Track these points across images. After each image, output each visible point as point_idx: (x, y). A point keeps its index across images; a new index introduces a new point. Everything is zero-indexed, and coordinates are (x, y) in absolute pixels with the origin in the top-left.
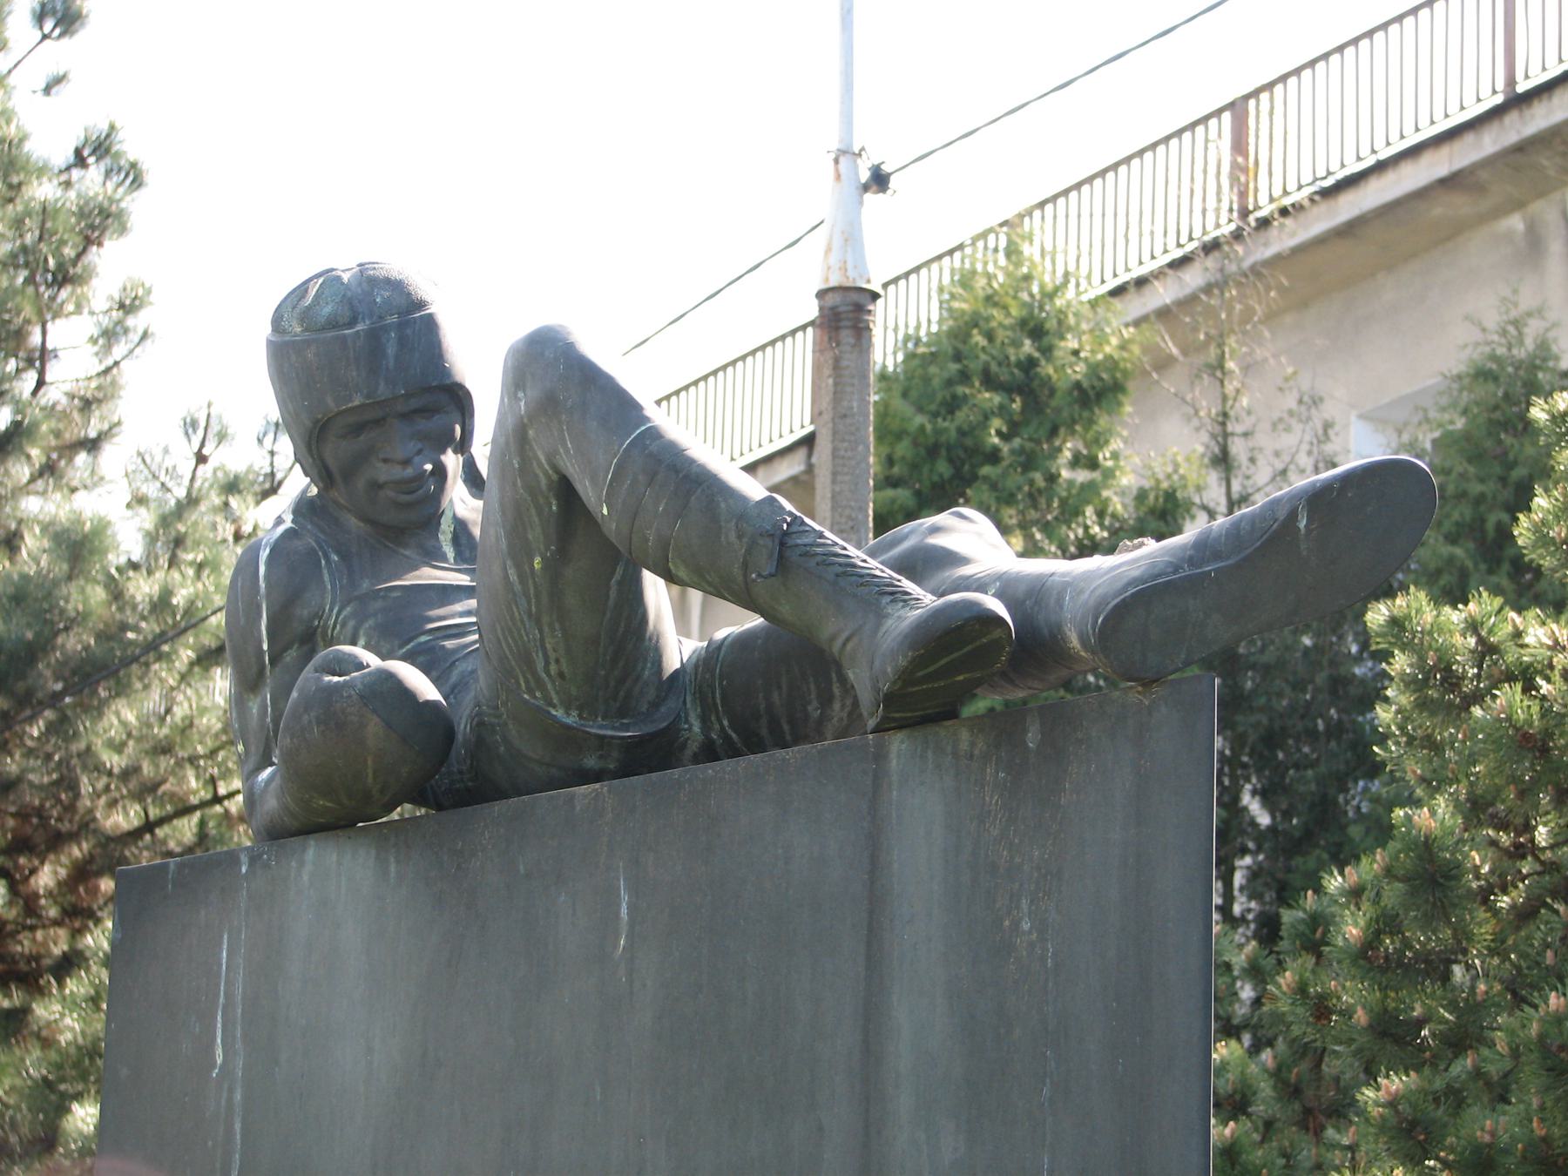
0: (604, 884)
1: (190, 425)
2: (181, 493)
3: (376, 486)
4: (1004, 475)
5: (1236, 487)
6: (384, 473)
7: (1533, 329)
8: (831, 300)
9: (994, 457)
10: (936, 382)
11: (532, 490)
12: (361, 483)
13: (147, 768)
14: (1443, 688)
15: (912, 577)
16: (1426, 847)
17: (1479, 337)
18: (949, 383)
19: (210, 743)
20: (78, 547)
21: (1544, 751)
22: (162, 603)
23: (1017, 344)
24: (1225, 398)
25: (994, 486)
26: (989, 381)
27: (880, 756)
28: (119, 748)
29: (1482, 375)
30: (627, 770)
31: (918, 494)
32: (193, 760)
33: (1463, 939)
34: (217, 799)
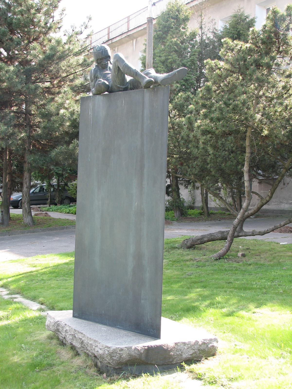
0: (122, 100)
1: (72, 26)
2: (71, 35)
3: (102, 64)
4: (173, 30)
5: (203, 31)
6: (103, 63)
7: (242, 10)
8: (148, 19)
9: (172, 28)
10: (166, 18)
11: (116, 67)
12: (101, 64)
13: (67, 69)
14: (212, 69)
15: (147, 76)
16: (208, 86)
17: (234, 12)
18: (167, 18)
19: (75, 66)
20: (58, 42)
21: (221, 77)
22: (69, 49)
23: (176, 13)
24: (202, 20)
25: (172, 32)
26: (172, 18)
27: (144, 91)
28: (64, 67)
29: (235, 16)
30: (124, 91)
31: (163, 32)
32: (72, 68)
33: (212, 96)
34: (76, 73)
